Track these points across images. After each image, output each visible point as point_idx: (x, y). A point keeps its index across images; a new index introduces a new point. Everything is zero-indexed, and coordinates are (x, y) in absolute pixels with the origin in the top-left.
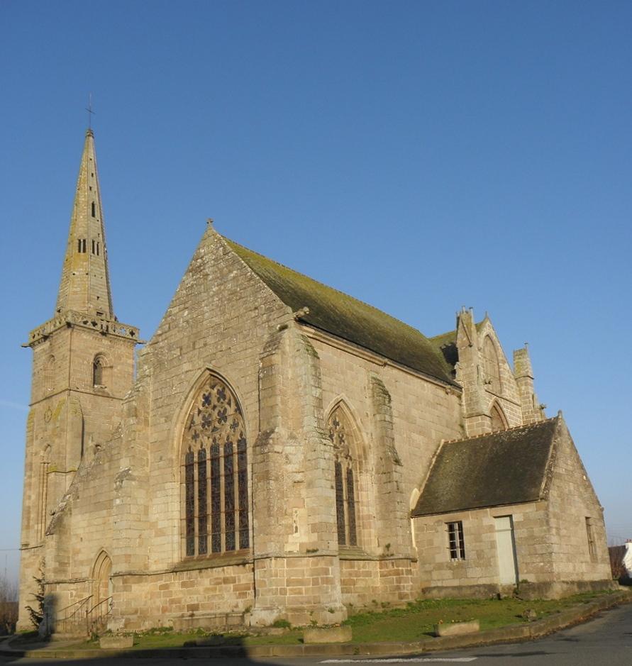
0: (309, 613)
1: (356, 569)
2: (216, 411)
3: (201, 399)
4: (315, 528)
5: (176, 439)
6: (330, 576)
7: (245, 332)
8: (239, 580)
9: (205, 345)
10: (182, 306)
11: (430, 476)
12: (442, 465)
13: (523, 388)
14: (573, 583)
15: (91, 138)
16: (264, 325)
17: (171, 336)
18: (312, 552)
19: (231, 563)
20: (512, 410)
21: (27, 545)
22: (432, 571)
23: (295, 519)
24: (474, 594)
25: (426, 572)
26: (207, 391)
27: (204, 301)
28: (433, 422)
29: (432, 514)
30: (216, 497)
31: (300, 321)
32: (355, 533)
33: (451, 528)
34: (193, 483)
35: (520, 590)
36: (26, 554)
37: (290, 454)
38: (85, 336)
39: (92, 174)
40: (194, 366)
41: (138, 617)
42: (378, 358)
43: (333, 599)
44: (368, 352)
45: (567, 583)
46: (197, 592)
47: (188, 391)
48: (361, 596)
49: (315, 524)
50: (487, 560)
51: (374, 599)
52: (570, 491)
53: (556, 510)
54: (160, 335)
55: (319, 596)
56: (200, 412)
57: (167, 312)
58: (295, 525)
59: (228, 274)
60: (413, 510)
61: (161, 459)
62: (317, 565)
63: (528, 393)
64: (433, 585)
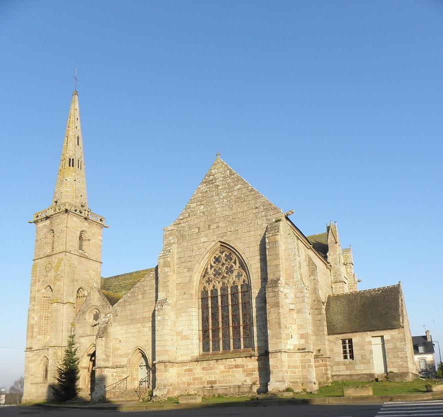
2: (225, 267)
4: (302, 336)
5: (195, 282)
8: (247, 366)
9: (218, 227)
13: (349, 269)
15: (76, 96)
18: (302, 350)
19: (242, 356)
21: (31, 348)
24: (360, 379)
29: (334, 334)
30: (225, 318)
33: (344, 342)
34: (228, 306)
35: (388, 376)
36: (30, 354)
38: (75, 219)
41: (173, 388)
47: (205, 254)
49: (303, 334)
50: (367, 360)
54: (182, 219)
55: (306, 375)
56: (212, 267)
57: (187, 206)
61: (185, 293)
62: (305, 357)
63: (351, 273)
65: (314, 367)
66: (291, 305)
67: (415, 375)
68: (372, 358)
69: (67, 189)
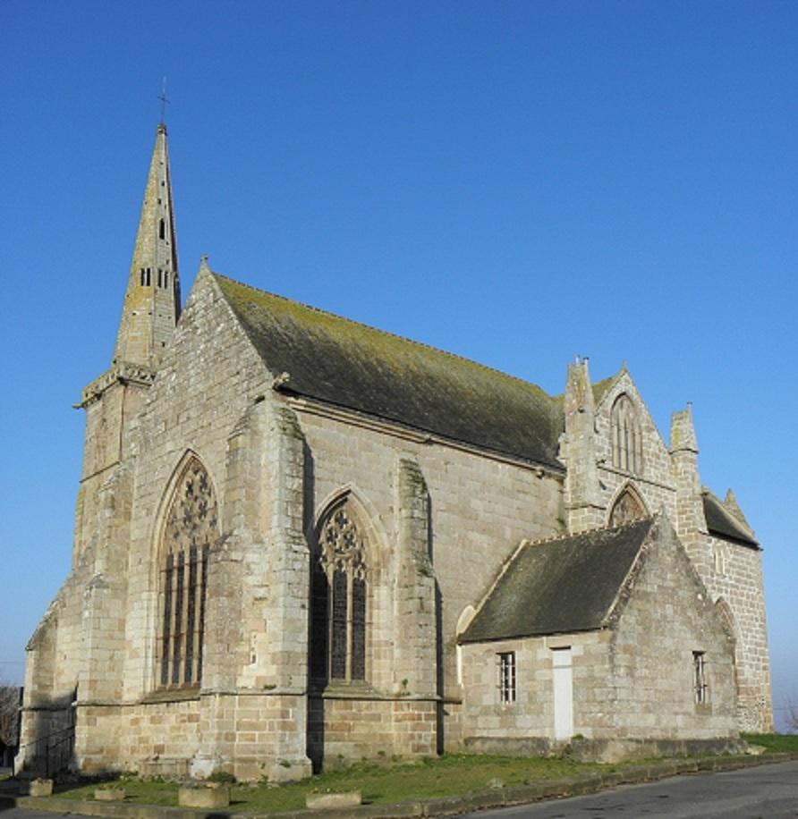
0: (260, 766)
1: (354, 710)
3: (185, 488)
6: (291, 719)
7: (226, 404)
10: (171, 368)
11: (495, 589)
12: (513, 576)
14: (650, 741)
15: (163, 135)
16: (243, 395)
17: (158, 406)
20: (658, 495)
22: (478, 716)
23: (253, 645)
25: (471, 717)
26: (190, 477)
27: (190, 362)
28: (509, 516)
29: (481, 641)
31: (282, 390)
32: (364, 664)
37: (254, 563)
39: (163, 184)
40: (176, 445)
42: (414, 433)
43: (291, 749)
44: (397, 426)
45: (638, 741)
46: (163, 731)
48: (361, 747)
50: (540, 706)
51: (382, 749)
52: (664, 617)
53: (631, 642)
54: (149, 405)
56: (182, 503)
58: (252, 654)
59: (215, 329)
60: (460, 635)
62: (274, 705)
64: (477, 735)
65: (393, 719)
66: (257, 589)
67: (67, 768)
68: (552, 701)
69: (134, 334)
